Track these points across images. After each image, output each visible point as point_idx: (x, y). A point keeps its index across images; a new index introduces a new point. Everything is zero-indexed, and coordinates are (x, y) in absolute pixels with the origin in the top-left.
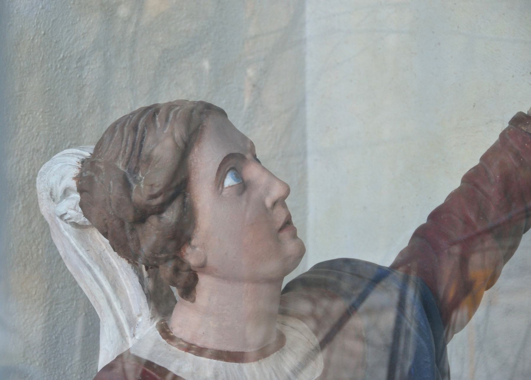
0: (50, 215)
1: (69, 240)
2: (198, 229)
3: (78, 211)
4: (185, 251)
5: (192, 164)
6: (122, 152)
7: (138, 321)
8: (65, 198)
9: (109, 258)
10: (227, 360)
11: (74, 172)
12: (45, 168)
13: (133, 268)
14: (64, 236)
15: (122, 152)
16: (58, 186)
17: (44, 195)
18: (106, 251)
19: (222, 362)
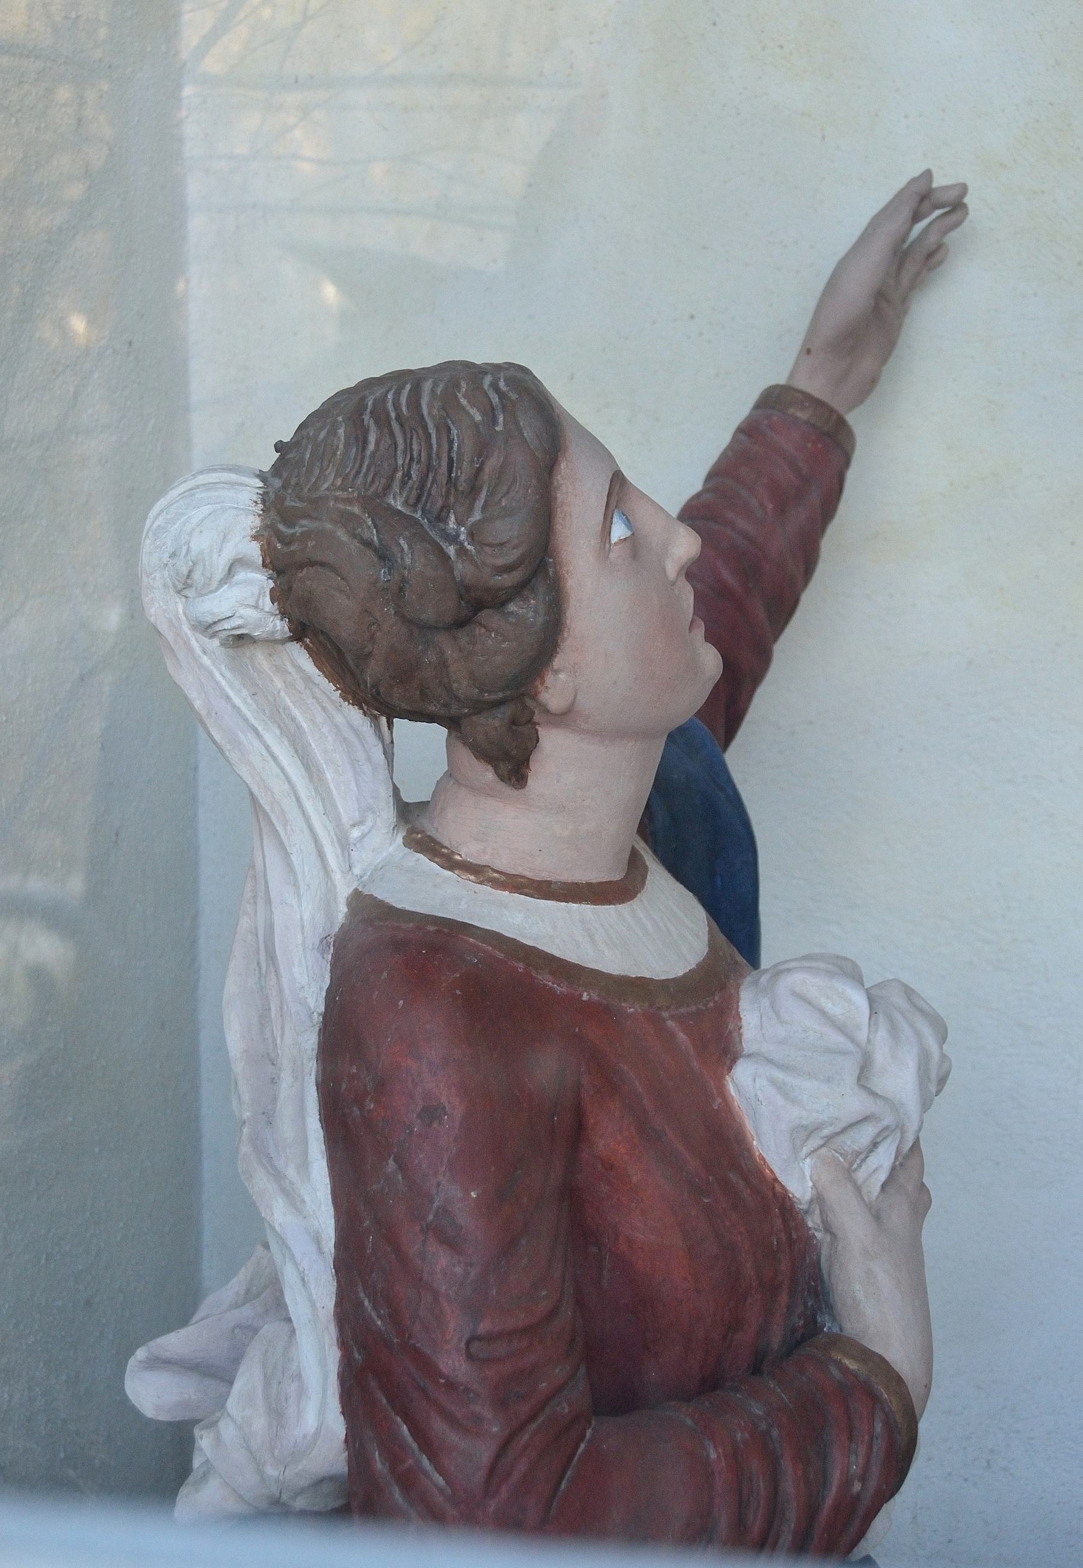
0: (170, 621)
1: (211, 673)
2: (566, 635)
3: (262, 610)
4: (543, 683)
5: (558, 495)
6: (399, 475)
7: (351, 836)
8: (226, 583)
9: (289, 706)
10: (595, 902)
11: (249, 523)
12: (169, 517)
13: (372, 724)
14: (201, 666)
15: (399, 475)
16: (215, 556)
17: (157, 578)
18: (282, 693)
19: (588, 906)
